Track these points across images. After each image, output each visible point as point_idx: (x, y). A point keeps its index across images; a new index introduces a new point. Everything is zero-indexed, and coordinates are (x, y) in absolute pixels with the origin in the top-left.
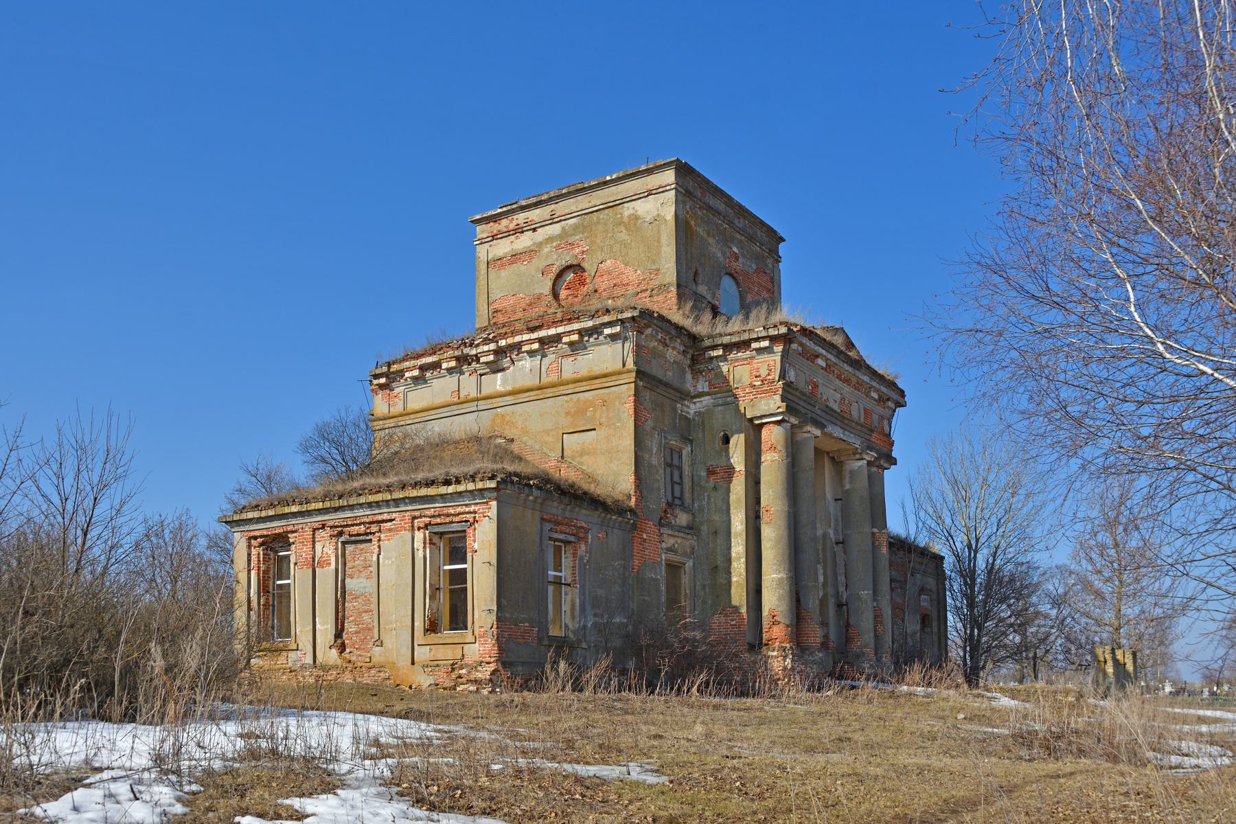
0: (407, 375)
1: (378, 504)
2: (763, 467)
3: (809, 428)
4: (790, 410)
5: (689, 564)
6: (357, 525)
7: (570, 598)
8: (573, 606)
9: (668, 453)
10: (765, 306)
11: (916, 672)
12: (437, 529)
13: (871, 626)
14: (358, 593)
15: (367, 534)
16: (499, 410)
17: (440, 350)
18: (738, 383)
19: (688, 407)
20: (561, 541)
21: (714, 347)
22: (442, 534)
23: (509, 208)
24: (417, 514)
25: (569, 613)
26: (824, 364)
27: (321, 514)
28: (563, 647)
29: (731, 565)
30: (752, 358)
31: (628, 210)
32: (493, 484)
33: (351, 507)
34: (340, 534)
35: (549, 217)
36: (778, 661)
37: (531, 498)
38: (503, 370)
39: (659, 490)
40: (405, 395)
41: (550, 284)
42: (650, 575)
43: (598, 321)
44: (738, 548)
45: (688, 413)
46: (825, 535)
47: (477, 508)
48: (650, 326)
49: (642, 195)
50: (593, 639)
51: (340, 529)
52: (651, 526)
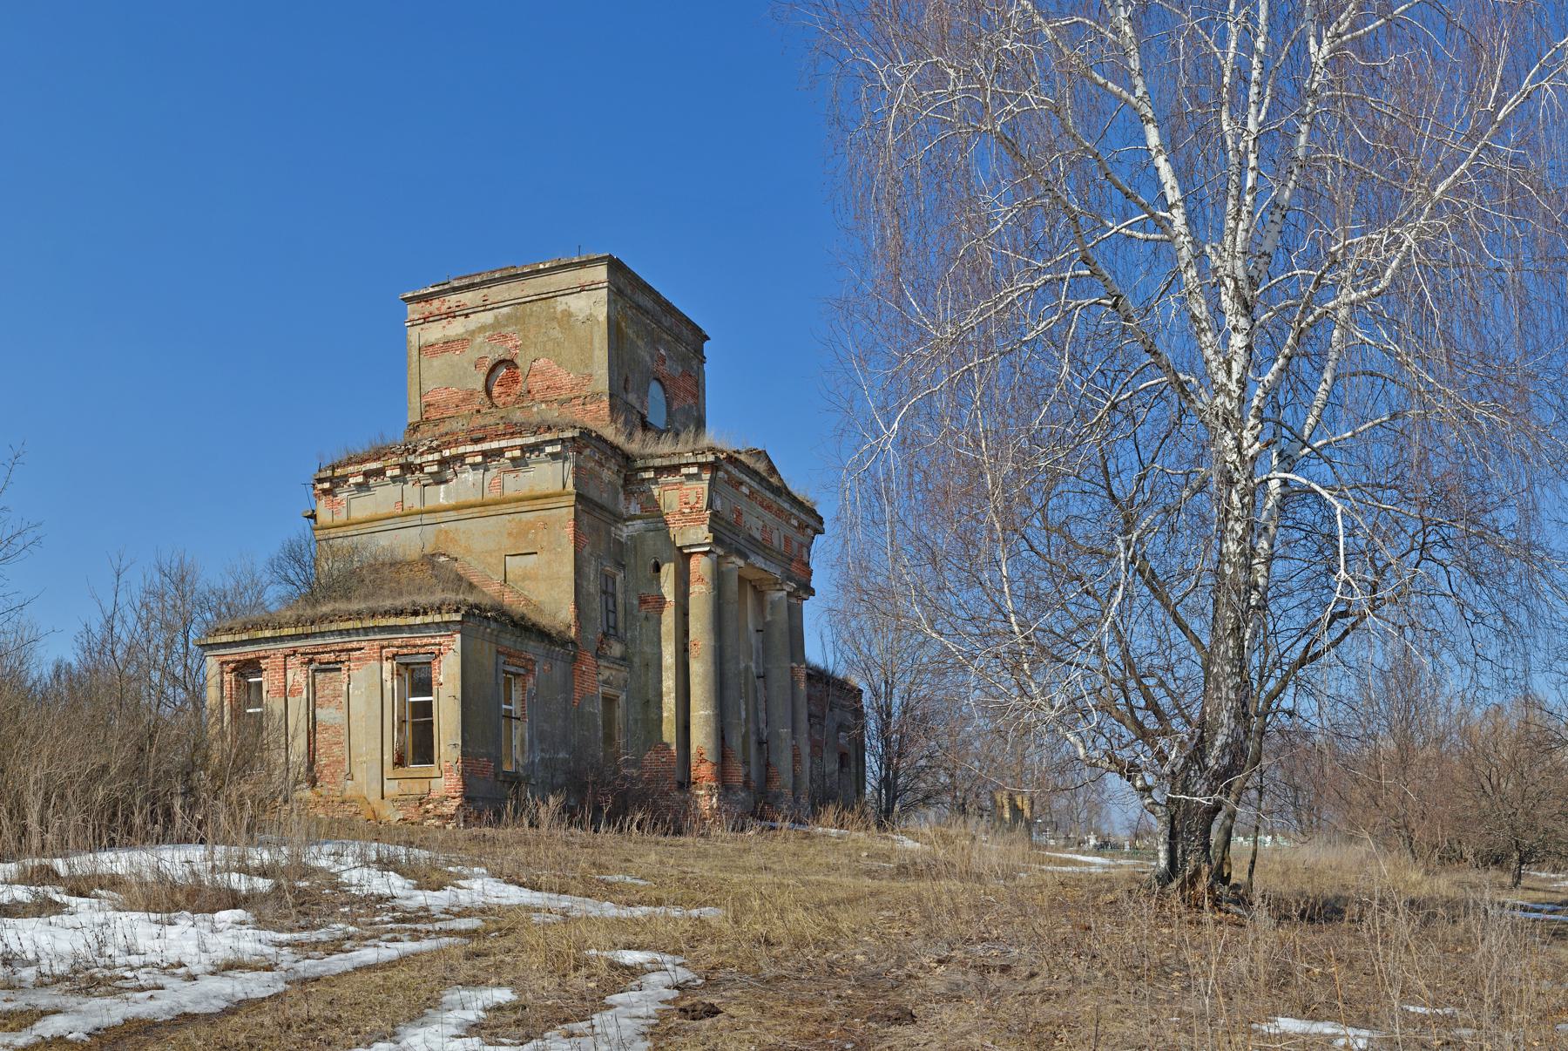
0: (352, 480)
1: (348, 632)
2: (691, 598)
3: (733, 559)
4: (717, 541)
5: (623, 697)
6: (329, 652)
7: (519, 733)
8: (523, 740)
9: (603, 579)
10: (692, 428)
11: (830, 813)
12: (404, 660)
13: (790, 766)
14: (328, 724)
15: (337, 662)
16: (442, 525)
17: (384, 456)
18: (668, 509)
19: (621, 530)
20: (512, 673)
21: (646, 469)
22: (408, 664)
23: (441, 288)
24: (385, 643)
25: (518, 747)
26: (747, 492)
27: (292, 640)
28: (514, 780)
29: (662, 699)
30: (681, 483)
31: (561, 304)
32: (458, 617)
33: (322, 634)
34: (311, 661)
35: (481, 303)
36: (706, 800)
37: (488, 630)
38: (446, 482)
39: (597, 619)
40: (349, 502)
41: (483, 379)
42: (588, 709)
43: (540, 438)
44: (669, 683)
45: (621, 536)
46: (747, 668)
47: (442, 640)
48: (588, 447)
49: (575, 290)
50: (540, 774)
51: (310, 656)
52: (589, 658)
